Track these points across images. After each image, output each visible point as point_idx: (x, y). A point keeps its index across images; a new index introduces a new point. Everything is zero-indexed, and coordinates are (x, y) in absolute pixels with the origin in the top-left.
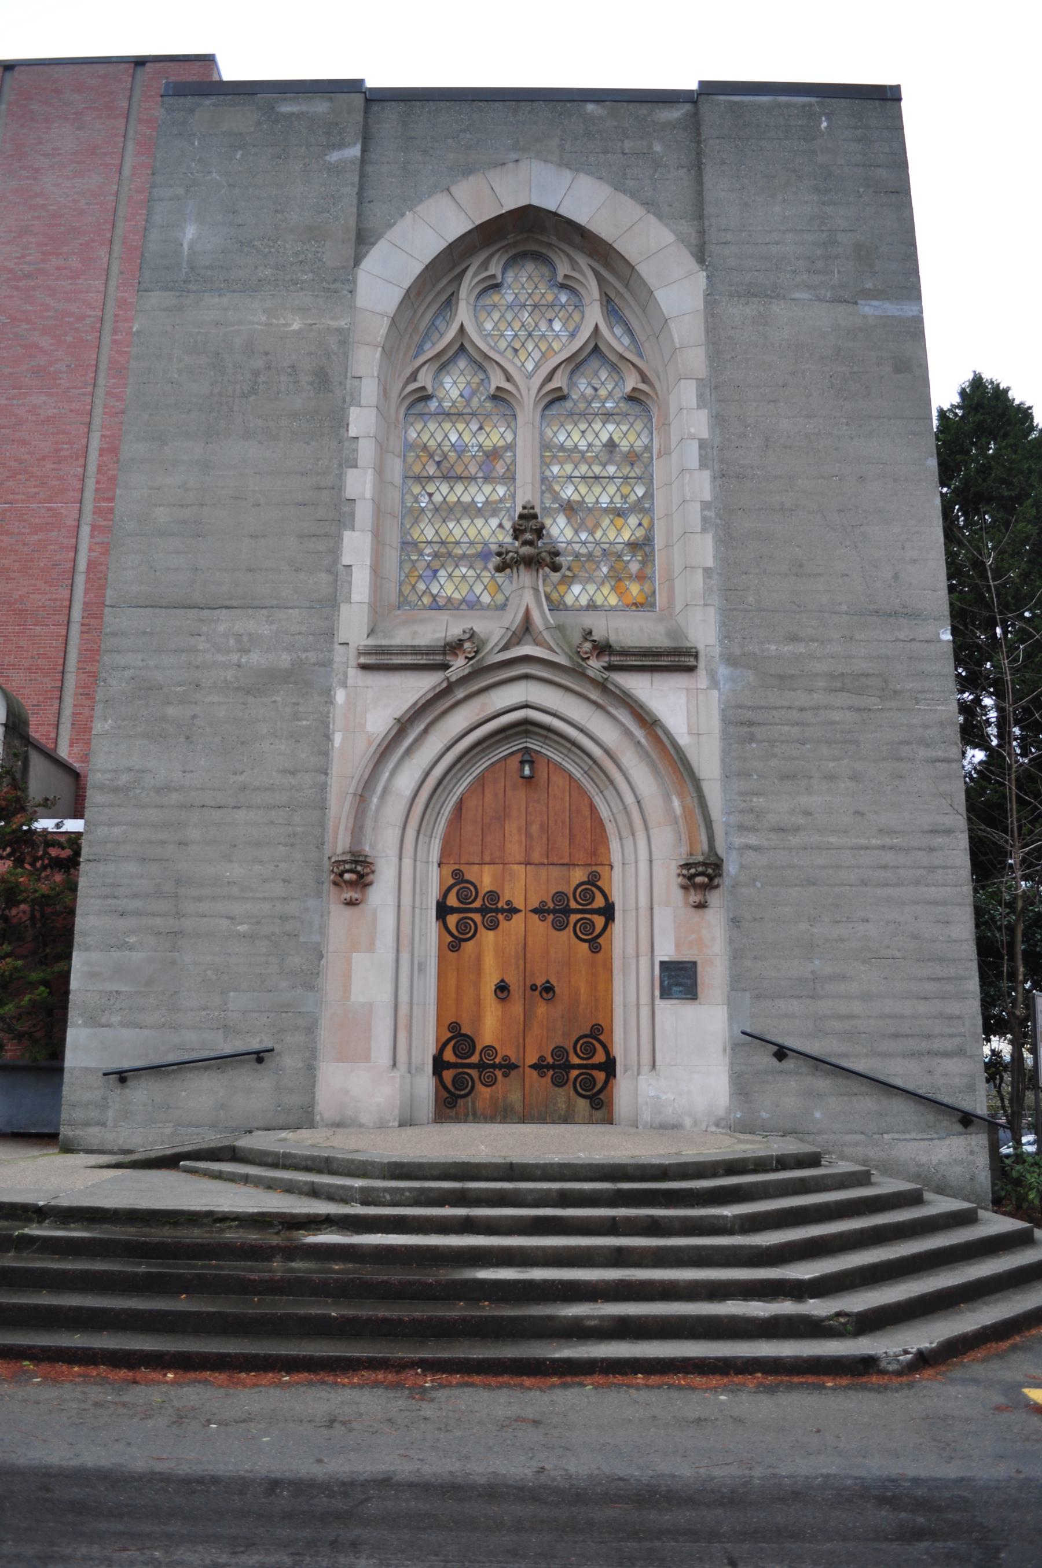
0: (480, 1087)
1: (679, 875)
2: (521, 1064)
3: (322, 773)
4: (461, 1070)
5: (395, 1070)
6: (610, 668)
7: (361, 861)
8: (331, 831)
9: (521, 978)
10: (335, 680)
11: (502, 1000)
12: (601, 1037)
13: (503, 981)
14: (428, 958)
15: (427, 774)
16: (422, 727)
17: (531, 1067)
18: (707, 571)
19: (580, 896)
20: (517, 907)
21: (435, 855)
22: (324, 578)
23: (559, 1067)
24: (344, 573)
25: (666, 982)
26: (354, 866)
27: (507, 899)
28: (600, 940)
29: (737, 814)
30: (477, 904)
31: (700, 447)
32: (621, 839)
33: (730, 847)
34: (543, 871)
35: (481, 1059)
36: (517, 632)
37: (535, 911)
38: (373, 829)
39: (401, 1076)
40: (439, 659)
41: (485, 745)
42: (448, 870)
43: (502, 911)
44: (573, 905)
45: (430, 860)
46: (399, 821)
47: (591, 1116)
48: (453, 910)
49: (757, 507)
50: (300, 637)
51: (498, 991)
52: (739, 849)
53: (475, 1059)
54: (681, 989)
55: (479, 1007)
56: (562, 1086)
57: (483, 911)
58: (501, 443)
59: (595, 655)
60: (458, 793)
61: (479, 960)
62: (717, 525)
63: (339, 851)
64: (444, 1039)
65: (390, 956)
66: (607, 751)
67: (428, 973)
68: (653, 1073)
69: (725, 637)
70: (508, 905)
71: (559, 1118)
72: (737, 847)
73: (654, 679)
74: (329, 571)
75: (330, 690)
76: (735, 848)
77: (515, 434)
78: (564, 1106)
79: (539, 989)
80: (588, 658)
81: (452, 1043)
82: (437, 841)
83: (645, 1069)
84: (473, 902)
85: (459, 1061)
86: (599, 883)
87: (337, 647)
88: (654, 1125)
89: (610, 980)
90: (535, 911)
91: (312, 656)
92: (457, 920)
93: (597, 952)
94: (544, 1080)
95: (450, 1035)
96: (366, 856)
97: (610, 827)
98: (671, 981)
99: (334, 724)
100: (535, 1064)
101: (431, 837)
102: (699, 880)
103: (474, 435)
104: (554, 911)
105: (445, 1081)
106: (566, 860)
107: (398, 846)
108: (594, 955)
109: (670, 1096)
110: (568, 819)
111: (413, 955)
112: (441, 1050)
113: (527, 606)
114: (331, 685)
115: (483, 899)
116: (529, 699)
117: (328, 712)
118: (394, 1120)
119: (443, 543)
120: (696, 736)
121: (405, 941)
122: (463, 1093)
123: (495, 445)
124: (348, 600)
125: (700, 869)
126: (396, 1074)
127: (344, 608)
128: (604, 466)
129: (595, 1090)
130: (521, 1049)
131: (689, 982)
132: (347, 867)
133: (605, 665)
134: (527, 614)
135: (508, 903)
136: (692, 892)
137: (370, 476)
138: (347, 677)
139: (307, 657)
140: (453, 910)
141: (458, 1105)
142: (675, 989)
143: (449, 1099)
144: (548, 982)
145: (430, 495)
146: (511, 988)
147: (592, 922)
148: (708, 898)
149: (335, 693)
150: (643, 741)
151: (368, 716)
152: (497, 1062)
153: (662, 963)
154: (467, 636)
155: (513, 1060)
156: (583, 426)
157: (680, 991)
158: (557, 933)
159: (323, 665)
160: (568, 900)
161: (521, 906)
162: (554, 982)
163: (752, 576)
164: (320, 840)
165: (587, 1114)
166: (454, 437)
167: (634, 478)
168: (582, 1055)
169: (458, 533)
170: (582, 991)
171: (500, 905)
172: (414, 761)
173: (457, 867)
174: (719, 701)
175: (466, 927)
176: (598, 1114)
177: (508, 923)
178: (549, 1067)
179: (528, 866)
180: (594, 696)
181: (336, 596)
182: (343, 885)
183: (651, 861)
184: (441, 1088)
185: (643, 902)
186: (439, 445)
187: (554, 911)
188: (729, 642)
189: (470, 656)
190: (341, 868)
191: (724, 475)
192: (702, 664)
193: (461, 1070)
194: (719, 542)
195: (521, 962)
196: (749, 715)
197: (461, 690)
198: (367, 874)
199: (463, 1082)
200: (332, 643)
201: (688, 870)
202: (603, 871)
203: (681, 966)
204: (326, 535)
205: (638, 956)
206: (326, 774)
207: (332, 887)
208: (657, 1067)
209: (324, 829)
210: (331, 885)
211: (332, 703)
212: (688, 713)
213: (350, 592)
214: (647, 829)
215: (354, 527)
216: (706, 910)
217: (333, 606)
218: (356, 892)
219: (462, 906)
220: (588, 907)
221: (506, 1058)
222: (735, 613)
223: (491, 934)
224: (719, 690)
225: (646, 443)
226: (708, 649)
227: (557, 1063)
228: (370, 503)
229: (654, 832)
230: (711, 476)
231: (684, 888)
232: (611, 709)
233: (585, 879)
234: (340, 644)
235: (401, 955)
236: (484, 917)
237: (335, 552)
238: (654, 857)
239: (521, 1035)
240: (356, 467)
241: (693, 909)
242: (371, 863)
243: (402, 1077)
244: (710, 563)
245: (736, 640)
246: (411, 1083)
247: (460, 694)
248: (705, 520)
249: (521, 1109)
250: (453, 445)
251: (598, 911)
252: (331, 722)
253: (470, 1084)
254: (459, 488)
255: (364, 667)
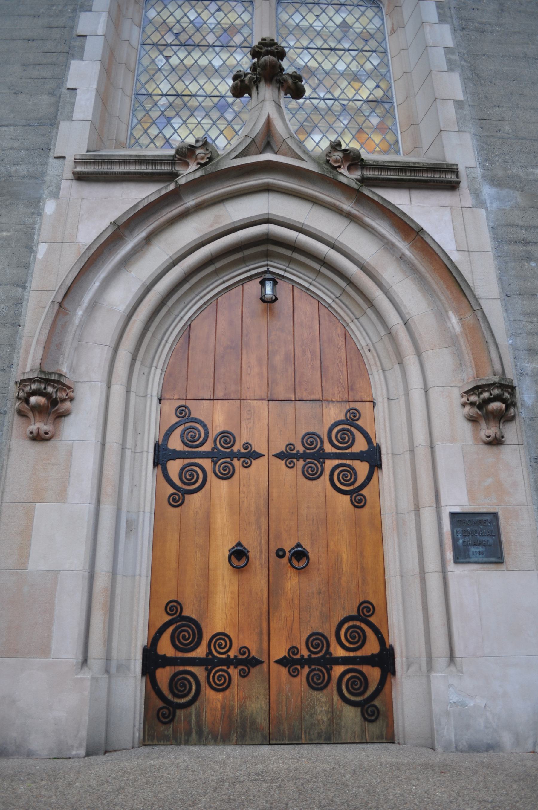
0: (208, 693)
1: (464, 405)
2: (264, 658)
3: (18, 286)
4: (181, 668)
5: (86, 669)
6: (364, 181)
7: (54, 381)
8: (22, 351)
9: (264, 542)
10: (46, 192)
11: (239, 569)
12: (372, 619)
13: (239, 544)
14: (141, 513)
15: (147, 290)
16: (143, 234)
17: (279, 662)
18: (458, 103)
19: (336, 437)
20: (258, 450)
21: (155, 389)
22: (45, 100)
23: (317, 661)
24: (68, 96)
25: (461, 541)
26: (43, 386)
27: (244, 441)
28: (364, 492)
29: (524, 335)
30: (207, 447)
31: (438, 7)
32: (384, 371)
33: (522, 373)
34: (289, 407)
35: (210, 652)
36: (256, 141)
37: (280, 456)
38: (76, 349)
39: (92, 678)
40: (167, 168)
41: (218, 265)
42: (170, 407)
43: (239, 455)
44: (328, 448)
45: (149, 392)
46: (109, 339)
47: (363, 731)
48: (176, 455)
49: (501, 54)
50: (11, 151)
51: (233, 558)
52: (532, 375)
53: (201, 652)
54: (481, 549)
55: (208, 580)
56: (321, 689)
57: (213, 455)
58: (239, 21)
59: (346, 168)
60: (186, 318)
61: (208, 516)
62: (462, 66)
63: (28, 369)
64: (159, 625)
65: (87, 508)
66: (364, 268)
67: (140, 535)
68: (452, 668)
69: (486, 160)
70: (246, 448)
71: (319, 736)
72: (530, 373)
73: (412, 196)
74: (52, 94)
75: (39, 201)
76: (527, 374)
77: (252, 15)
78: (325, 718)
79: (288, 555)
80: (339, 167)
81: (171, 629)
82: (159, 371)
83: (441, 662)
84: (202, 444)
85: (180, 655)
86: (359, 423)
87: (52, 160)
88: (460, 747)
89: (380, 543)
90: (280, 456)
91: (23, 169)
92: (181, 466)
93: (363, 506)
94: (297, 680)
95: (167, 618)
96: (61, 375)
97: (369, 358)
98: (467, 539)
99: (39, 235)
100: (285, 657)
101: (151, 367)
102: (496, 405)
103: (213, 15)
104: (304, 456)
105: (160, 685)
106: (318, 396)
107: (107, 369)
108: (358, 510)
109: (480, 702)
110: (318, 350)
111: (119, 509)
112: (155, 640)
113: (269, 116)
114: (41, 197)
115: (215, 441)
116: (271, 212)
117: (34, 224)
118: (80, 745)
119: (178, 95)
120: (467, 253)
121: (108, 489)
122: (183, 701)
123: (232, 23)
124: (70, 118)
125: (496, 392)
126: (86, 675)
127: (64, 126)
128: (339, 42)
129: (368, 694)
130: (265, 637)
131: (490, 540)
132: (34, 386)
133: (359, 177)
134: (269, 123)
135: (247, 445)
136: (483, 424)
137: (103, 18)
138: (60, 189)
139: (16, 171)
140: (176, 455)
141: (176, 718)
142: (473, 549)
143: (165, 711)
144: (299, 545)
145: (167, 58)
146: (250, 554)
147: (353, 469)
148: (503, 430)
149: (44, 204)
150: (408, 253)
151: (80, 227)
152: (232, 657)
153: (453, 515)
154: (200, 143)
155: (254, 653)
156: (317, 10)
157: (480, 553)
158: (309, 482)
159: (35, 178)
160: (322, 442)
161: (262, 450)
162: (307, 545)
163: (505, 109)
164: (7, 361)
165: (358, 729)
166: (192, 15)
167: (369, 51)
168: (347, 644)
169: (194, 88)
170: (345, 556)
171: (235, 449)
172: (132, 273)
173: (182, 403)
174: (487, 219)
175: (192, 475)
176: (373, 729)
177: (246, 470)
178: (303, 662)
179: (270, 402)
180: (347, 206)
181: (56, 116)
182: (30, 414)
183: (426, 391)
184: (153, 694)
185: (421, 438)
186: (178, 22)
187: (304, 456)
188: (491, 164)
189: (203, 162)
190: (27, 389)
191: (463, 29)
192: (464, 184)
193: (181, 668)
194: (465, 81)
195: (264, 521)
196: (522, 234)
197: (192, 197)
198: (63, 400)
199: (185, 686)
200: (48, 157)
201: (479, 396)
202: (364, 408)
203: (478, 518)
204: (53, 64)
205: (417, 509)
206: (24, 288)
207: (17, 418)
208: (458, 660)
209: (14, 349)
210: (16, 415)
211: (40, 214)
212: (454, 229)
213: (72, 112)
214: (419, 354)
215: (83, 56)
216: (502, 448)
217: (52, 125)
218: (46, 424)
219: (187, 449)
220: (347, 451)
221: (243, 650)
222: (492, 139)
223: (225, 483)
224: (487, 209)
225: (378, 26)
226: (469, 170)
227: (313, 656)
228: (101, 40)
229: (429, 356)
230: (451, 29)
231: (473, 420)
232: (368, 220)
233: (342, 417)
234: (56, 158)
235: (102, 506)
236: (215, 463)
237: (61, 78)
238: (430, 384)
239: (265, 614)
240: (90, 11)
241: (486, 447)
242: (69, 388)
243: (94, 679)
244: (460, 96)
245: (498, 164)
246: (109, 688)
247: (190, 202)
248: (450, 62)
249: (265, 724)
250: (191, 22)
251: (360, 456)
252: (36, 233)
253: (194, 687)
254: (196, 54)
255: (80, 177)
